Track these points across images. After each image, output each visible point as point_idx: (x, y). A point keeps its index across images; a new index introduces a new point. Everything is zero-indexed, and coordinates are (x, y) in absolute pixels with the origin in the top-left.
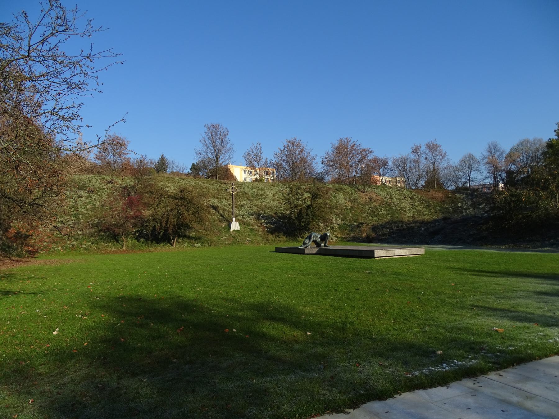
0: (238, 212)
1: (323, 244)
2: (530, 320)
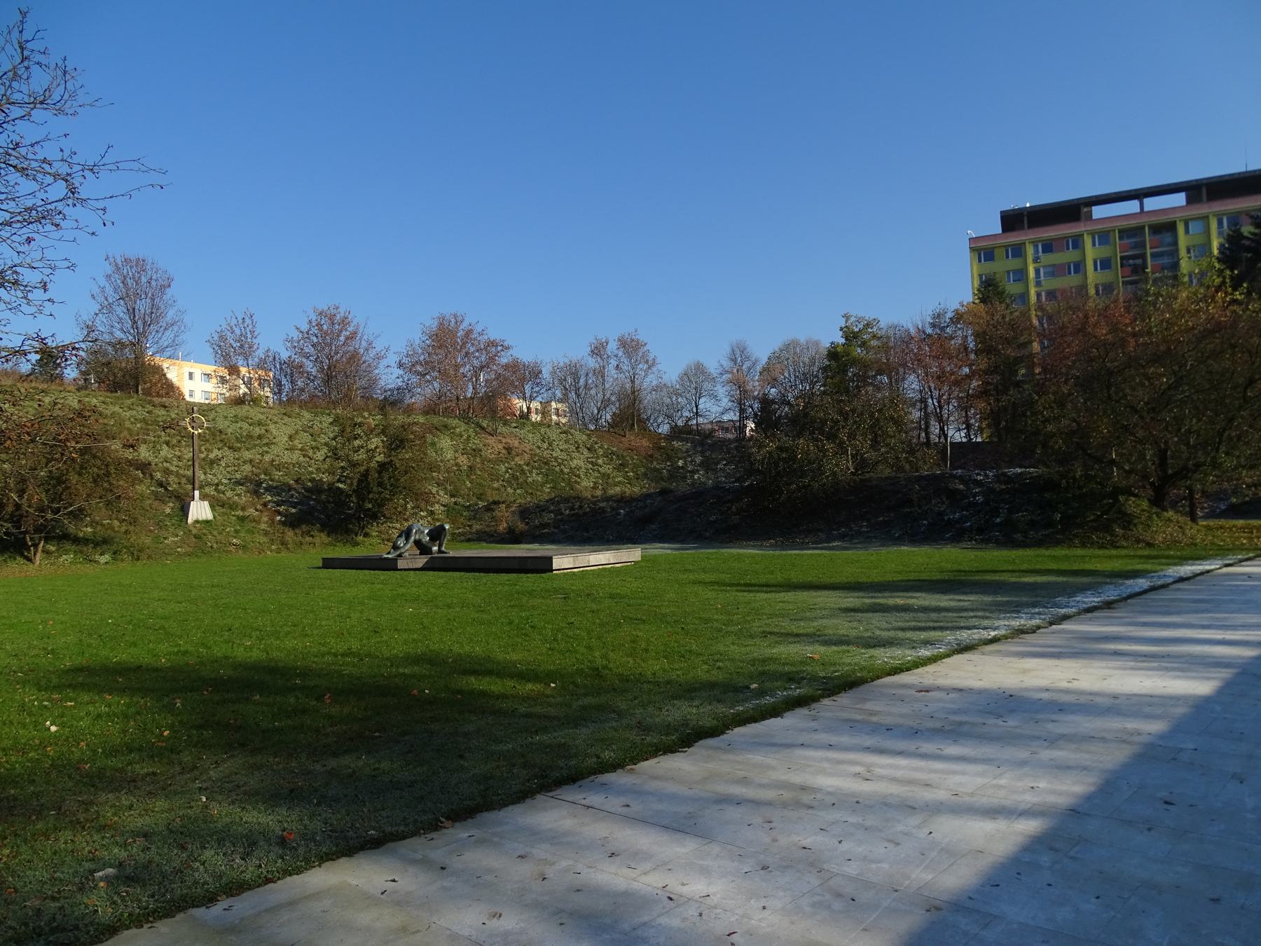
0: (203, 477)
1: (435, 548)
2: (848, 643)
